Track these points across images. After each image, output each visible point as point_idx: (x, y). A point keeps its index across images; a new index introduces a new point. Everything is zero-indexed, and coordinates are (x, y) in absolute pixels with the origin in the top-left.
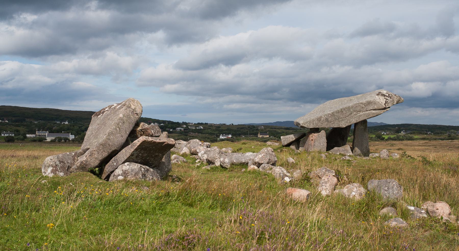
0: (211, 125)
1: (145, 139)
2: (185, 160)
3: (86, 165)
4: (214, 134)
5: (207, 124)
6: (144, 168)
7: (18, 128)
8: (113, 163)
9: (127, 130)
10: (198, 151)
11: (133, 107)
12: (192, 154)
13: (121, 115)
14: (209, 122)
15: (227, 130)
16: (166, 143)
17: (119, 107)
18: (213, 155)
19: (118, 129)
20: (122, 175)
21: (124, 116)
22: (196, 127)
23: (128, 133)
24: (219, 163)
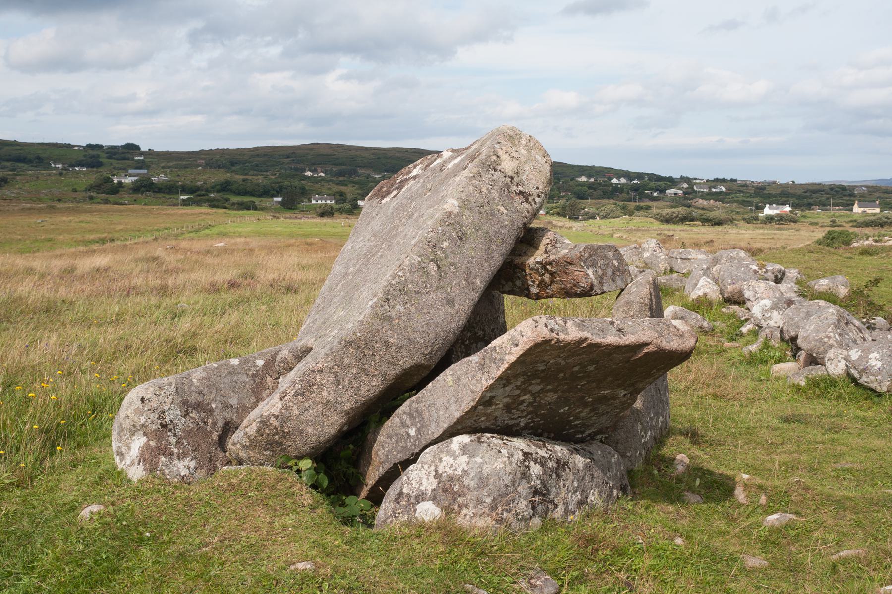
0: (745, 185)
1: (545, 333)
2: (705, 325)
3: (284, 435)
4: (749, 204)
5: (736, 181)
6: (542, 463)
7: (343, 188)
8: (404, 425)
9: (476, 271)
10: (747, 294)
11: (508, 166)
12: (729, 301)
13: (452, 205)
14: (741, 177)
15: (780, 195)
16: (650, 349)
17: (456, 166)
18: (817, 331)
19: (432, 268)
20: (434, 499)
21: (465, 205)
22: (710, 188)
23: (480, 283)
24: (842, 365)
